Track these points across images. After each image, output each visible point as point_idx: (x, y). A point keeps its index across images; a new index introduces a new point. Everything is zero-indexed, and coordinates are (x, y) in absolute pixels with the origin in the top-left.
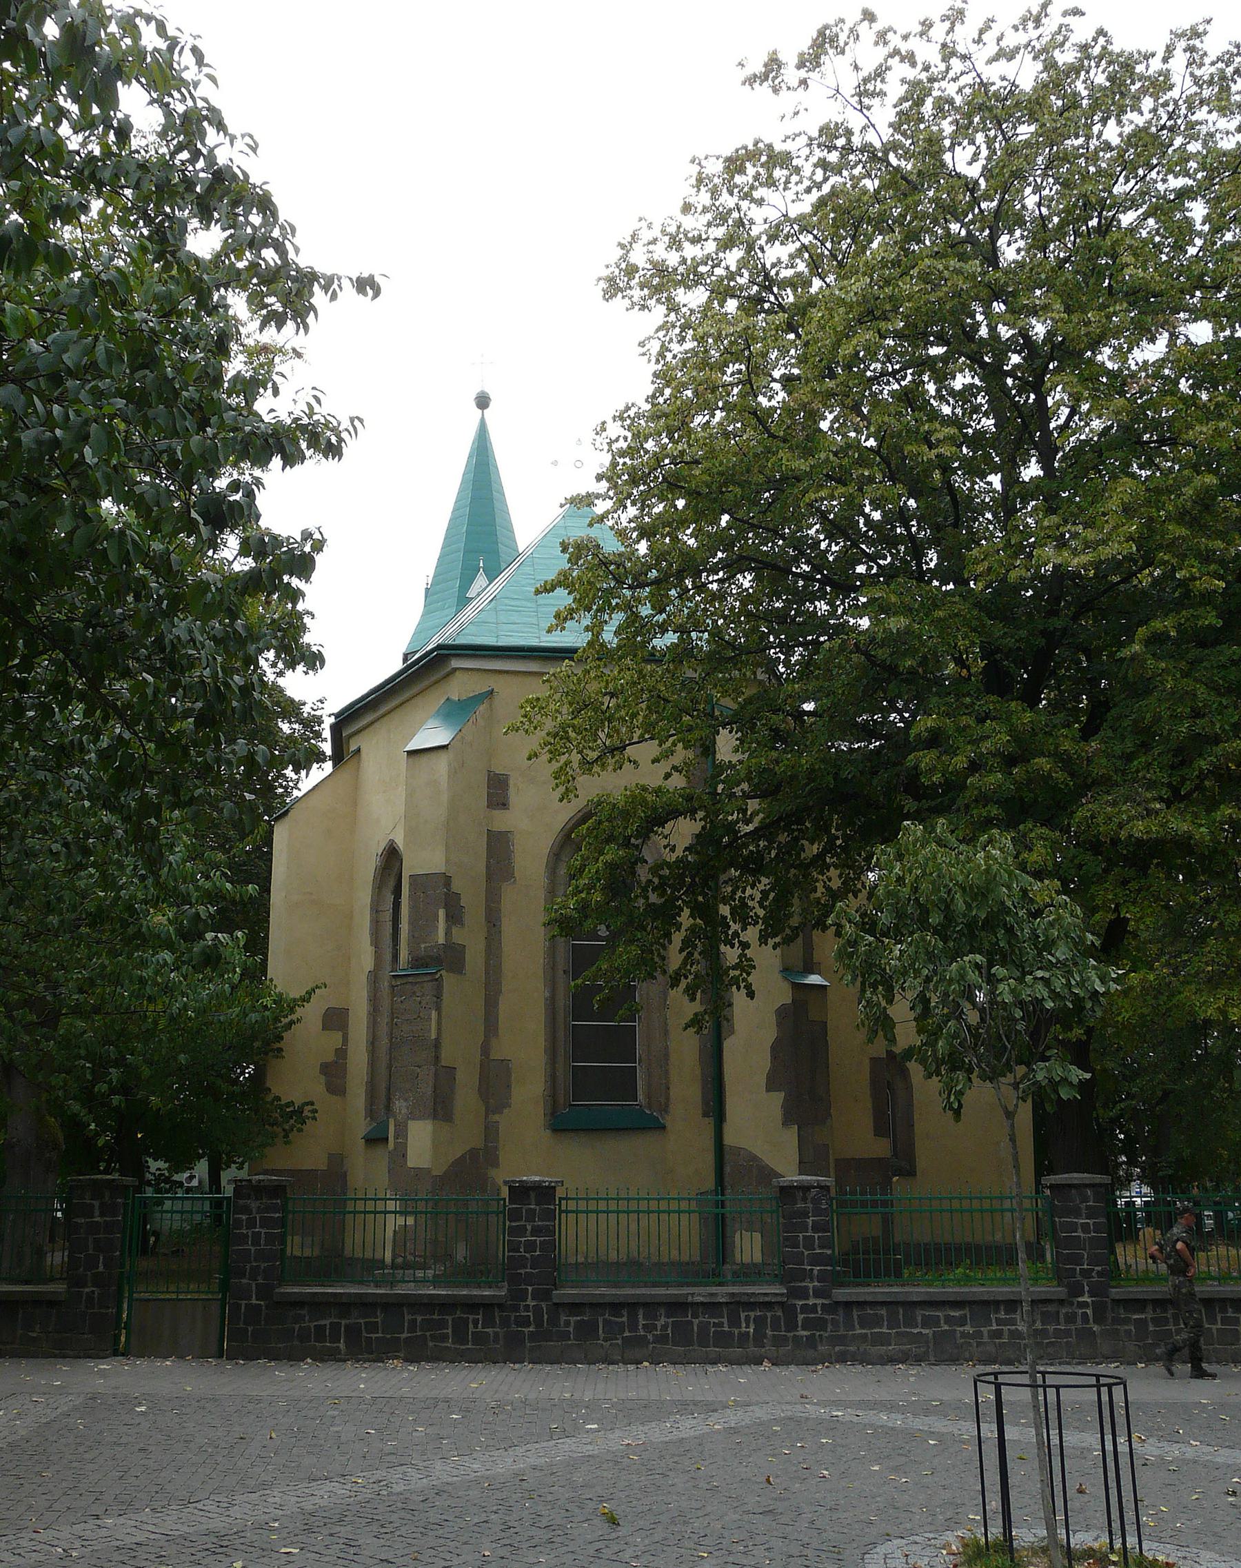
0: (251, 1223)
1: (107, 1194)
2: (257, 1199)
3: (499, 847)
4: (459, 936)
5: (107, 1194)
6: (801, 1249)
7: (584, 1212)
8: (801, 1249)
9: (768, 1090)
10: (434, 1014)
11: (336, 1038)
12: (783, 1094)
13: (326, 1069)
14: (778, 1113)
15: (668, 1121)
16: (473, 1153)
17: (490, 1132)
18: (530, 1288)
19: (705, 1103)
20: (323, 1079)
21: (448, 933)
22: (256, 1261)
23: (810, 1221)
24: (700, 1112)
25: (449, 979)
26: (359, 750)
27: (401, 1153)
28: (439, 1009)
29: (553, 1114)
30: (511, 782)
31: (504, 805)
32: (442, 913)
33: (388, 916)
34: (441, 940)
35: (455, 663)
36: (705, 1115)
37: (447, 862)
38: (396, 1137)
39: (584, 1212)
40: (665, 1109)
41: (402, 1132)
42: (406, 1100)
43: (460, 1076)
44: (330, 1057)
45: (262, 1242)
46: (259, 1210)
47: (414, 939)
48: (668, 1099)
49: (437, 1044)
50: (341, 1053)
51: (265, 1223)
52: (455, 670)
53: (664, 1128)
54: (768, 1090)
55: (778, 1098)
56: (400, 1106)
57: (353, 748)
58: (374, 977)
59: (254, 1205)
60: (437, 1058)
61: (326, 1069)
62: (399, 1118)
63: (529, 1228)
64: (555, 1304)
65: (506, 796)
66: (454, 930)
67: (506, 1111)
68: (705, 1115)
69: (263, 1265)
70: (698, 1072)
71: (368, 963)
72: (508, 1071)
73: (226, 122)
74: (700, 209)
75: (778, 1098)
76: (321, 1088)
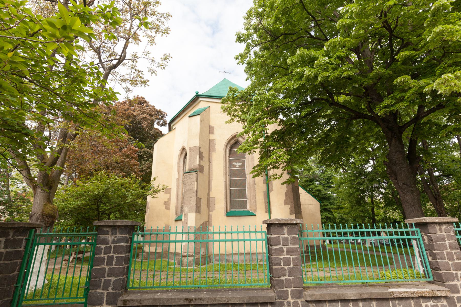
0: (108, 250)
1: (11, 234)
2: (112, 234)
3: (211, 143)
4: (202, 163)
5: (11, 234)
6: (447, 260)
7: (254, 240)
8: (447, 260)
9: (285, 204)
10: (196, 183)
11: (168, 196)
13: (165, 203)
14: (288, 211)
15: (256, 214)
18: (289, 290)
19: (266, 209)
21: (199, 162)
22: (108, 276)
23: (447, 242)
25: (200, 174)
28: (197, 182)
30: (215, 128)
32: (198, 156)
33: (182, 165)
34: (198, 163)
35: (200, 99)
36: (266, 212)
37: (200, 143)
38: (185, 217)
39: (254, 240)
40: (256, 211)
41: (186, 216)
43: (202, 201)
44: (166, 200)
45: (114, 263)
46: (114, 242)
47: (190, 163)
49: (197, 192)
50: (169, 199)
51: (116, 249)
52: (200, 101)
54: (285, 204)
55: (288, 207)
56: (186, 209)
58: (178, 180)
59: (110, 238)
60: (197, 195)
61: (165, 203)
62: (186, 212)
63: (285, 249)
64: (307, 301)
68: (266, 212)
69: (113, 279)
70: (264, 201)
71: (177, 177)
72: (215, 201)
73: (157, 108)
75: (288, 207)
76: (164, 208)
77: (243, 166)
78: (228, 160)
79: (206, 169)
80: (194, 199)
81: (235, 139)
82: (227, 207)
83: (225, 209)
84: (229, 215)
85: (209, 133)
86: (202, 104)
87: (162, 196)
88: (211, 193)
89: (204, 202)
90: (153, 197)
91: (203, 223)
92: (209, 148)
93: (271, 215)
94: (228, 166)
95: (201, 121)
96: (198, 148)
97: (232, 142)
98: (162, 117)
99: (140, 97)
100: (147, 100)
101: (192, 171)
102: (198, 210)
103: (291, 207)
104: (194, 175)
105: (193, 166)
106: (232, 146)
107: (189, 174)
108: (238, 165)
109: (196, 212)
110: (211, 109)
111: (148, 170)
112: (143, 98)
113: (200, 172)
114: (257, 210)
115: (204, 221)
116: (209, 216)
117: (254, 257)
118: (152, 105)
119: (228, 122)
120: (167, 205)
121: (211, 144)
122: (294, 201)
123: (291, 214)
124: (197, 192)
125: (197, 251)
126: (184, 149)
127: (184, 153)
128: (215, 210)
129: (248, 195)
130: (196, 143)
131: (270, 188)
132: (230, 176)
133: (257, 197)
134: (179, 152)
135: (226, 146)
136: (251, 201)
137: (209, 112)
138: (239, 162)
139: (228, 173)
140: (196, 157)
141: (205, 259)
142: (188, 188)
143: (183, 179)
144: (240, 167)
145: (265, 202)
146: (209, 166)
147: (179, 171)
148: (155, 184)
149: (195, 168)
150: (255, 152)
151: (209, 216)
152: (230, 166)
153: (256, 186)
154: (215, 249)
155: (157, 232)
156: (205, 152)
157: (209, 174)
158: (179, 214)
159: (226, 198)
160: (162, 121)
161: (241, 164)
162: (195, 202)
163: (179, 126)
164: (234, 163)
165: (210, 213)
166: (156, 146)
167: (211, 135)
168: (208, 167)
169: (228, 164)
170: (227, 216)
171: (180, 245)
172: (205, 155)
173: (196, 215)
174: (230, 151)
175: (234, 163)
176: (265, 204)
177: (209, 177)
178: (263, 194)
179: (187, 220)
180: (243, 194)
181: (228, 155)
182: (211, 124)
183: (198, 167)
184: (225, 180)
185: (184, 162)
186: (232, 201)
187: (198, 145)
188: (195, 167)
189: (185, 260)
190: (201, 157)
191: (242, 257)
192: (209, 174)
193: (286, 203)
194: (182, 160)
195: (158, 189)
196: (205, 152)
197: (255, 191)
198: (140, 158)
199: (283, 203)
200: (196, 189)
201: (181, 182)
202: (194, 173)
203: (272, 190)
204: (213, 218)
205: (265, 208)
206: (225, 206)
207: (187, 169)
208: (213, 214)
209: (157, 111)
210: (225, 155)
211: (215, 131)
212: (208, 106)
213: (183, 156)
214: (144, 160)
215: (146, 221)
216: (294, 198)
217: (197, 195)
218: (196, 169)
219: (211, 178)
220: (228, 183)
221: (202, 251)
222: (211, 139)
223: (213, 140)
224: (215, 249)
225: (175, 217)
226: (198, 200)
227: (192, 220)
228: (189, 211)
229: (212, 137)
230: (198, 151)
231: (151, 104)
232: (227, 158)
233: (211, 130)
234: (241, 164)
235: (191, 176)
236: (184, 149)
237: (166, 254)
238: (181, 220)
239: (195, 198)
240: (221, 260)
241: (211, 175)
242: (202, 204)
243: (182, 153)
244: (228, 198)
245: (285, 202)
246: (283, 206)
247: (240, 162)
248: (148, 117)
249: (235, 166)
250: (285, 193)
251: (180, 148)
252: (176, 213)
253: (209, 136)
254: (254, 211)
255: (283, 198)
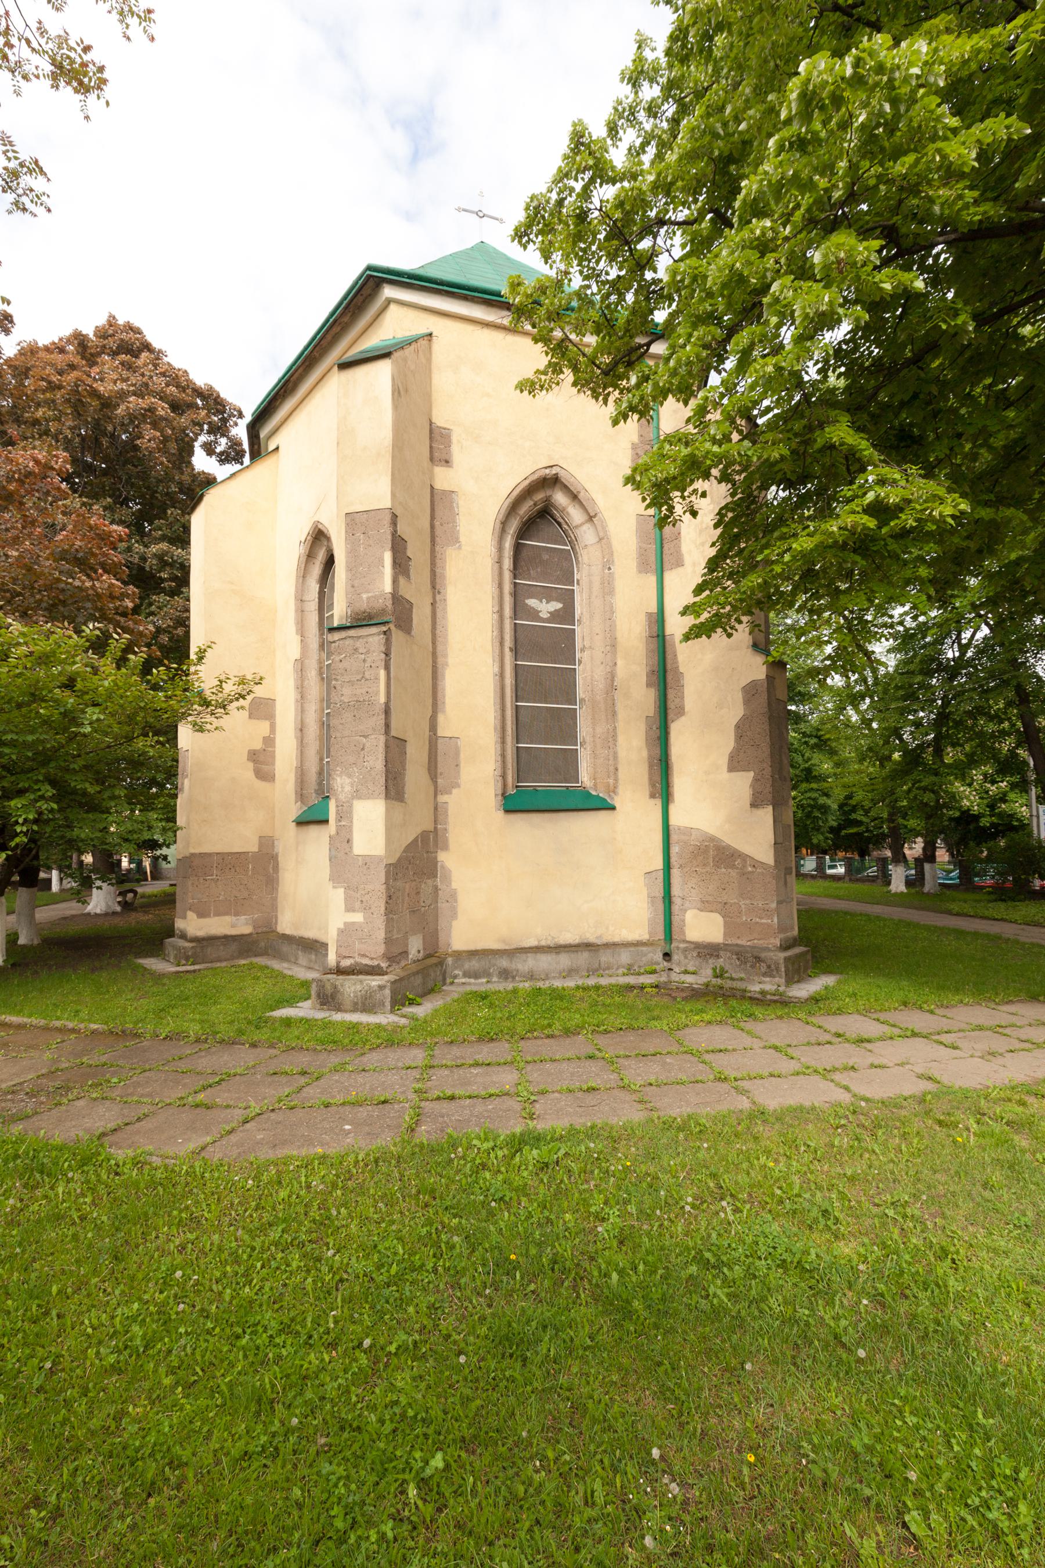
3: (439, 504)
4: (407, 591)
10: (382, 673)
11: (263, 728)
12: (752, 774)
13: (254, 756)
15: (617, 802)
16: (424, 835)
17: (438, 812)
19: (652, 784)
20: (251, 765)
21: (395, 582)
24: (648, 793)
26: (277, 448)
27: (343, 840)
28: (387, 668)
29: (503, 794)
30: (454, 438)
31: (447, 462)
32: (388, 557)
33: (313, 606)
34: (388, 588)
35: (388, 292)
36: (652, 796)
38: (340, 818)
40: (613, 790)
41: (345, 814)
42: (349, 776)
43: (410, 749)
44: (258, 745)
47: (352, 587)
48: (616, 780)
49: (387, 711)
50: (269, 741)
52: (389, 301)
53: (613, 808)
56: (342, 784)
57: (271, 447)
58: (300, 666)
60: (387, 726)
61: (254, 756)
62: (342, 797)
65: (449, 453)
66: (402, 580)
67: (454, 791)
68: (652, 796)
70: (645, 754)
71: (295, 652)
73: (200, 379)
74: (192, 1038)
76: (250, 774)
77: (567, 614)
78: (507, 587)
79: (420, 617)
80: (376, 744)
81: (539, 496)
82: (504, 776)
83: (500, 785)
84: (516, 803)
85: (432, 459)
86: (397, 320)
87: (237, 727)
88: (441, 718)
89: (416, 754)
90: (201, 730)
91: (416, 840)
92: (432, 527)
93: (673, 809)
94: (508, 611)
95: (398, 392)
96: (388, 518)
97: (526, 509)
98: (224, 421)
99: (121, 322)
100: (156, 344)
101: (361, 621)
102: (394, 788)
103: (756, 780)
104: (372, 638)
105: (365, 601)
106: (526, 529)
107: (352, 633)
108: (546, 608)
109: (387, 797)
110: (437, 346)
111: (180, 631)
112: (130, 328)
113: (398, 626)
114: (620, 790)
115: (419, 831)
116: (436, 809)
117: (605, 957)
118: (177, 365)
119: (529, 387)
120: (261, 761)
121: (438, 513)
122: (772, 755)
123: (754, 805)
124: (387, 711)
125: (396, 950)
126: (319, 536)
127: (321, 555)
128: (458, 786)
129: (584, 728)
130: (376, 492)
131: (671, 705)
132: (516, 651)
133: (621, 739)
134: (303, 550)
135: (504, 524)
136: (594, 755)
137: (429, 360)
138: (548, 595)
139: (508, 642)
140: (381, 561)
141: (422, 971)
142: (346, 694)
143: (320, 662)
144: (555, 616)
145: (650, 758)
146: (433, 604)
147: (301, 630)
148: (205, 676)
149: (371, 610)
150: (694, 514)
151: (436, 809)
152: (515, 615)
153: (618, 696)
154: (462, 934)
155: (230, 863)
156: (414, 535)
157: (434, 643)
158: (314, 799)
159: (503, 741)
160: (223, 441)
161: (559, 606)
162: (381, 756)
163: (297, 435)
164: (532, 602)
165: (442, 798)
166: (198, 521)
167: (439, 471)
168: (428, 610)
169: (508, 600)
170: (507, 811)
171: (324, 902)
172: (418, 551)
173: (387, 810)
174: (518, 548)
175: (532, 602)
176: (651, 766)
177: (434, 654)
178: (642, 727)
179: (350, 829)
180: (563, 726)
181: (507, 563)
182: (439, 421)
183: (389, 603)
184: (497, 670)
185: (321, 594)
186: (523, 755)
187: (388, 504)
188: (379, 604)
189: (351, 987)
190: (401, 565)
191: (564, 960)
192: (434, 643)
193: (735, 764)
194: (314, 587)
195: (220, 698)
196: (414, 535)
197: (614, 714)
198: (144, 580)
199: (724, 762)
200: (382, 699)
201: (312, 674)
202: (374, 630)
203: (681, 711)
204: (451, 819)
205: (650, 779)
206: (499, 772)
207: (339, 613)
208: (453, 801)
209: (198, 392)
210: (499, 562)
211: (457, 454)
212: (423, 330)
213: (317, 569)
214: (163, 591)
215: (181, 820)
216: (772, 745)
217: (387, 726)
218: (383, 611)
219: (440, 660)
220: (509, 680)
221: (415, 946)
222: (438, 486)
223: (449, 495)
224: (462, 934)
225: (294, 810)
226: (395, 749)
227: (370, 827)
228: (358, 795)
229: (443, 478)
230: (386, 530)
231: (176, 358)
232: (507, 576)
233: (437, 446)
234: (559, 606)
235: (359, 644)
236: (319, 536)
237: (264, 943)
238: (326, 822)
239: (382, 739)
240: (486, 974)
241: (439, 648)
242: (410, 765)
243: (310, 556)
244: (509, 739)
245: (732, 758)
246: (724, 775)
247: (558, 600)
248: (163, 409)
249: (534, 614)
250: (738, 727)
251: (302, 531)
252: (301, 796)
253: (432, 477)
254: (608, 793)
255: (729, 743)
